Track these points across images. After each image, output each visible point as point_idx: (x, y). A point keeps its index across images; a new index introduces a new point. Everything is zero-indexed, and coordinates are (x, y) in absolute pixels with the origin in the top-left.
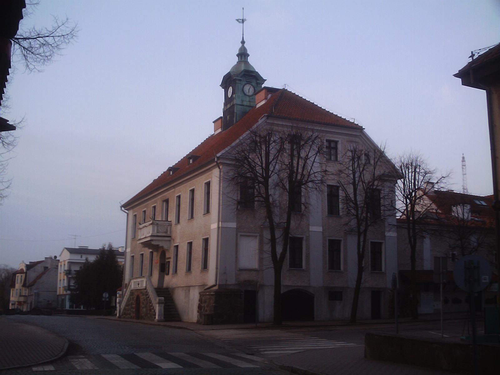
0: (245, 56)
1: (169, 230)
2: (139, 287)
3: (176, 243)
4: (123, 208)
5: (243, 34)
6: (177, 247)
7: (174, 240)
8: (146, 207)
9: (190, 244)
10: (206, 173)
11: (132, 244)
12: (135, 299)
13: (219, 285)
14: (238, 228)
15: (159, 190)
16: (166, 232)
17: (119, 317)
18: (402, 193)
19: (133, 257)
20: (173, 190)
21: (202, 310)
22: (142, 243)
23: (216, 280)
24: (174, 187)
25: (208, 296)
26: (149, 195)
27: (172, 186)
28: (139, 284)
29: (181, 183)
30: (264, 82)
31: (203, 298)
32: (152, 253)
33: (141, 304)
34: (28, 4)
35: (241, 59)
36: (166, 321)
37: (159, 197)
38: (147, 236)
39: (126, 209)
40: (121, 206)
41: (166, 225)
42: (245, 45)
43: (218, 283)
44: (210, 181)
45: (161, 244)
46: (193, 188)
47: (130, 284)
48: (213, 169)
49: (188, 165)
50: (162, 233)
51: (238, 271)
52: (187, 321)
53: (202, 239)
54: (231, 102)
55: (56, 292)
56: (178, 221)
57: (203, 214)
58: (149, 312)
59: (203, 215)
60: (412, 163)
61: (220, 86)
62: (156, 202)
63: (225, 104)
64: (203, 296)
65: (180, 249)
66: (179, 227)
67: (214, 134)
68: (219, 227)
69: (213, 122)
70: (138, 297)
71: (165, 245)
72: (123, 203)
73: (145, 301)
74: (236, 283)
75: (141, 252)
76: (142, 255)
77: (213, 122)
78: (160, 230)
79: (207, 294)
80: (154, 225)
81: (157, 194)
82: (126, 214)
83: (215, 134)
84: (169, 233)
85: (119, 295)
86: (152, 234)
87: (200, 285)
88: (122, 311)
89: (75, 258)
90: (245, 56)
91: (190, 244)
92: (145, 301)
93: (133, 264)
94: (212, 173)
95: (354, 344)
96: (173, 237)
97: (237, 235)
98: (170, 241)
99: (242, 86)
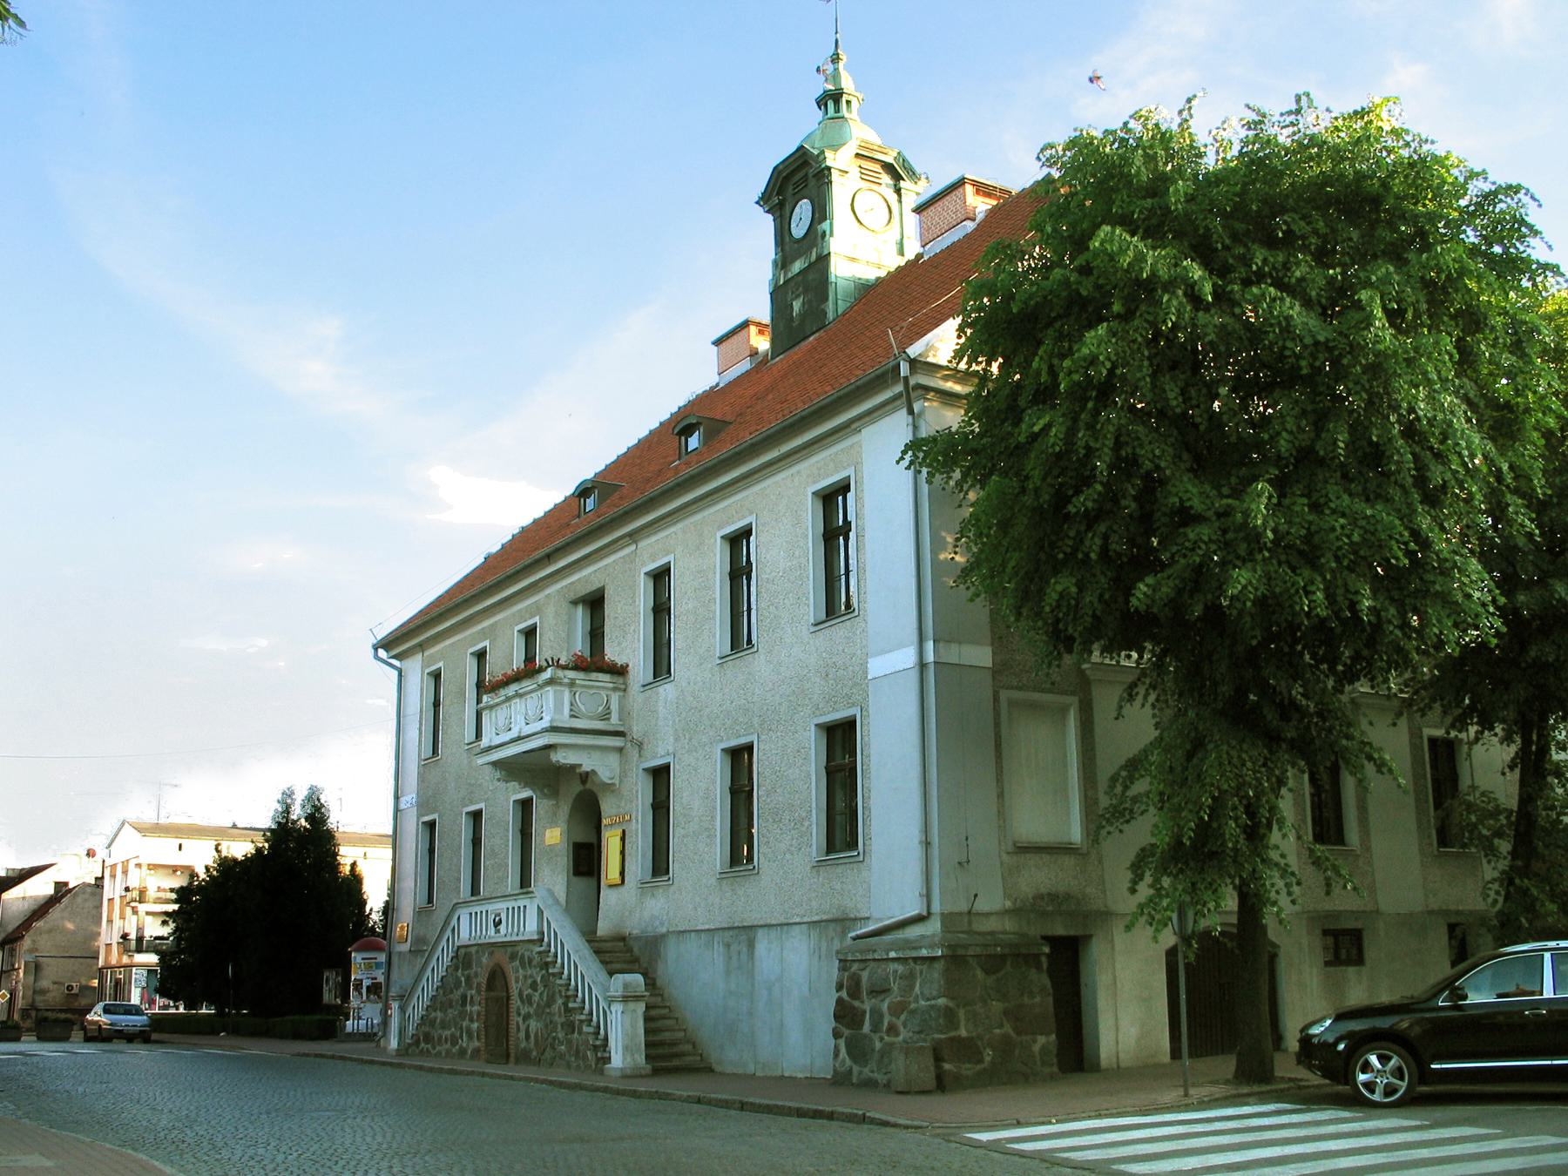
1: (614, 707)
2: (505, 934)
3: (654, 758)
4: (382, 653)
6: (660, 775)
7: (640, 745)
8: (483, 634)
9: (740, 757)
11: (422, 778)
12: (483, 979)
13: (947, 919)
14: (998, 671)
16: (606, 716)
17: (403, 1051)
19: (431, 825)
21: (867, 1028)
22: (495, 764)
23: (928, 896)
24: (633, 536)
25: (900, 968)
28: (497, 924)
31: (865, 975)
32: (525, 806)
33: (515, 1002)
36: (656, 1072)
37: (552, 589)
38: (522, 734)
40: (375, 642)
41: (603, 688)
43: (936, 907)
44: (670, 562)
45: (587, 762)
46: (530, 622)
47: (454, 921)
49: (579, 516)
50: (591, 718)
51: (1008, 853)
52: (779, 1073)
53: (813, 728)
54: (810, 249)
55: (97, 958)
56: (661, 666)
57: (812, 621)
58: (561, 1035)
59: (816, 625)
61: (757, 203)
62: (537, 610)
63: (782, 263)
64: (862, 965)
65: (676, 782)
66: (667, 691)
67: (717, 385)
68: (922, 666)
70: (497, 977)
71: (603, 766)
72: (383, 632)
73: (541, 988)
74: (1008, 904)
75: (472, 803)
76: (476, 816)
78: (582, 707)
79: (893, 954)
80: (561, 684)
81: (541, 579)
82: (396, 673)
83: (721, 385)
84: (614, 719)
85: (1520, 927)
86: (551, 721)
87: (816, 918)
88: (411, 1030)
91: (740, 757)
92: (541, 988)
93: (431, 851)
94: (859, 444)
96: (636, 730)
97: (996, 699)
98: (620, 750)
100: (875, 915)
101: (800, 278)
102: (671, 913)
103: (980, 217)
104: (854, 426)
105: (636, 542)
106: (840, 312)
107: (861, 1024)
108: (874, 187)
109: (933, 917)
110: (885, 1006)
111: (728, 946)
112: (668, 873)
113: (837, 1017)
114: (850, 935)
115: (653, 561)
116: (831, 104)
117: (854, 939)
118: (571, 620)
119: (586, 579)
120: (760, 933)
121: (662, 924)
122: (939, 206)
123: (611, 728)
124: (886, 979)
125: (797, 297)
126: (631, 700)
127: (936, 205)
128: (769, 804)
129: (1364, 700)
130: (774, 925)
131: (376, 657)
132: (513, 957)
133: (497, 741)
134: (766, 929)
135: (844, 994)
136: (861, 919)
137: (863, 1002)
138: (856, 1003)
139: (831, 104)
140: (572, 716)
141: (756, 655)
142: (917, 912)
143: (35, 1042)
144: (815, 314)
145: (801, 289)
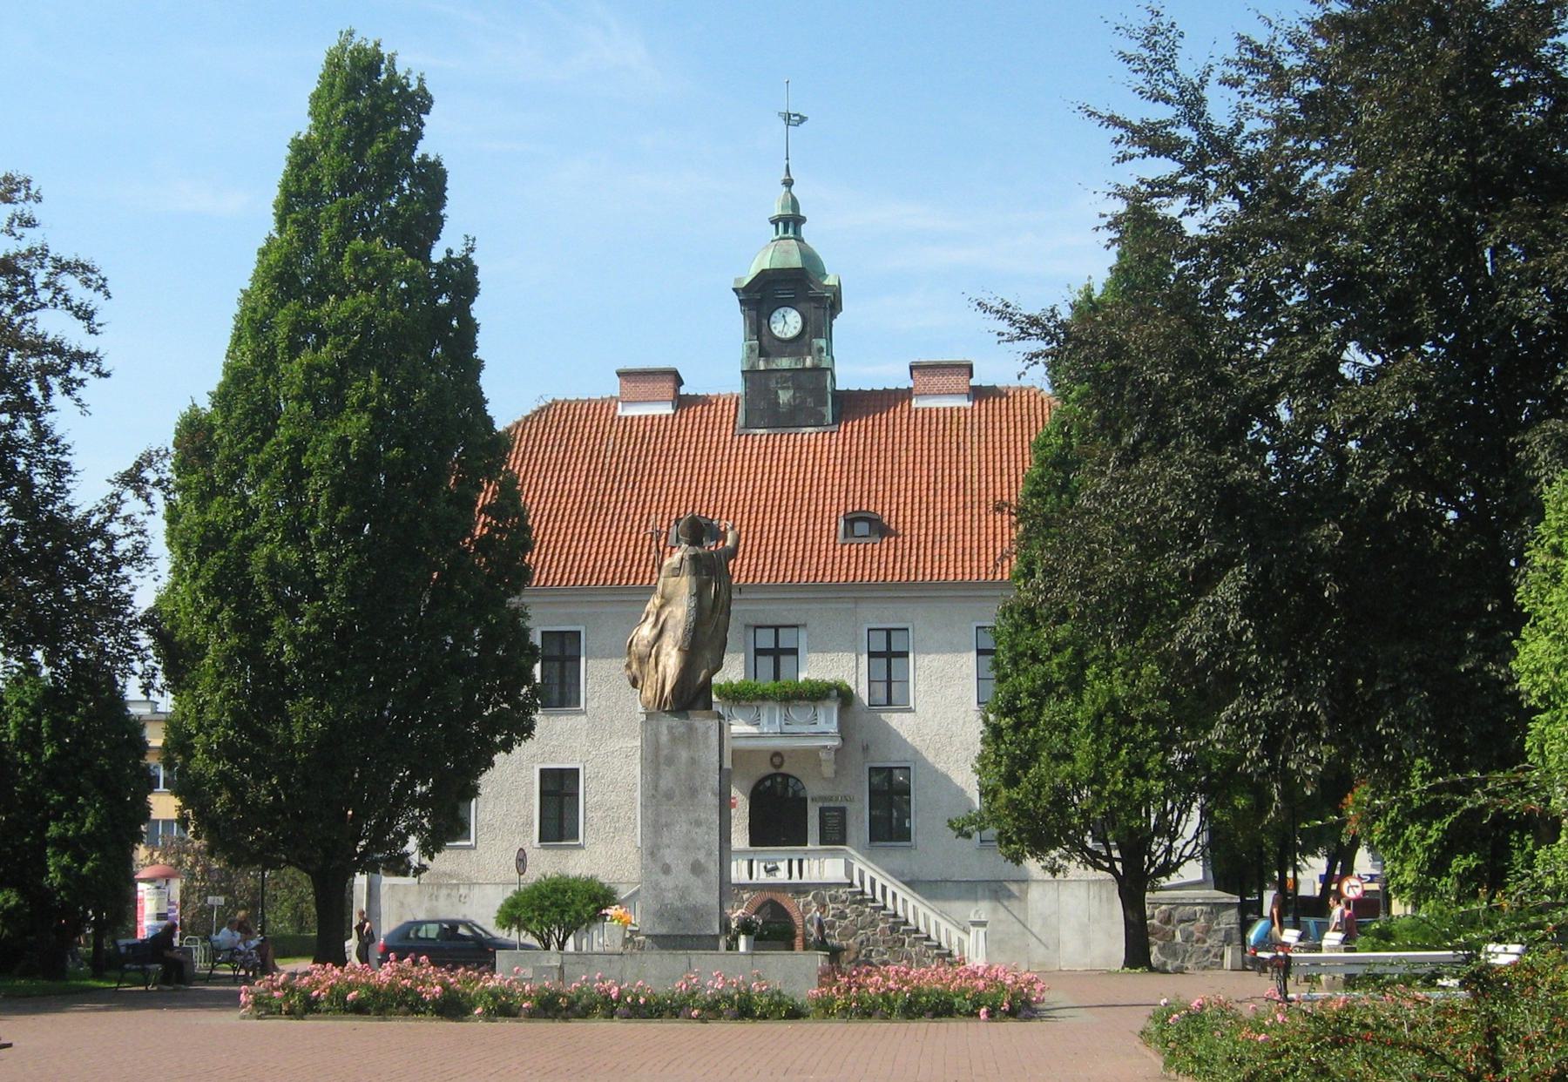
5: (788, 183)
69: (623, 374)
77: (620, 374)
89: (774, 607)
101: (789, 374)
139: (781, 224)
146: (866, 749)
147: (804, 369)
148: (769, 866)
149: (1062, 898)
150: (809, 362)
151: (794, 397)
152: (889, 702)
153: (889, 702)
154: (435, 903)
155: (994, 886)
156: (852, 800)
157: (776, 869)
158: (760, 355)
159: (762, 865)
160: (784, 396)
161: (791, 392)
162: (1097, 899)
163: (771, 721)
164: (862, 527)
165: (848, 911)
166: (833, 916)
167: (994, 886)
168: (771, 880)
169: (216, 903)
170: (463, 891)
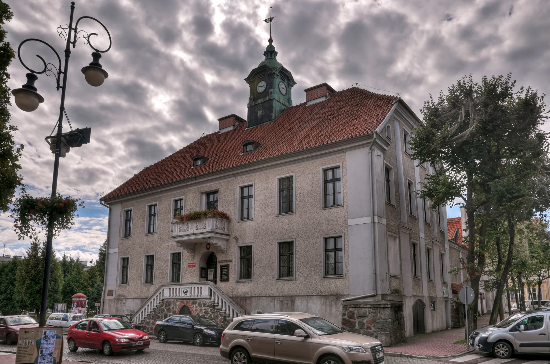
0: (271, 54)
4: (103, 202)
10: (333, 155)
15: (322, 150)
16: (224, 229)
18: (469, 336)
20: (234, 178)
22: (177, 242)
23: (376, 289)
26: (277, 161)
27: (234, 174)
29: (320, 155)
30: (294, 85)
34: (51, 134)
35: (268, 57)
39: (107, 203)
42: (273, 44)
43: (380, 292)
48: (348, 151)
50: (220, 229)
60: (70, 240)
82: (108, 209)
84: (226, 230)
89: (210, 184)
90: (271, 54)
95: (132, 351)
98: (227, 240)
99: (278, 83)
100: (351, 294)
101: (261, 105)
102: (252, 291)
103: (12, 107)
104: (343, 151)
105: (235, 177)
106: (276, 116)
107: (354, 326)
108: (283, 82)
109: (378, 295)
110: (365, 321)
111: (282, 301)
112: (251, 278)
113: (343, 324)
114: (342, 300)
115: (244, 183)
116: (269, 54)
117: (344, 301)
118: (201, 199)
119: (211, 186)
120: (297, 298)
121: (248, 294)
122: (317, 90)
123: (225, 233)
124: (366, 313)
125: (260, 110)
126: (232, 225)
127: (314, 90)
128: (300, 260)
129: (435, 242)
130: (303, 296)
131: (101, 203)
132: (194, 303)
133: (179, 234)
134: (301, 297)
135: (346, 317)
136: (345, 295)
137: (355, 320)
138: (352, 320)
139: (269, 54)
140: (216, 228)
141: (294, 215)
142: (373, 294)
143: (158, 342)
144: (267, 117)
145: (261, 108)
146: (237, 239)
147: (266, 101)
148: (185, 291)
149: (309, 304)
150: (267, 99)
151: (263, 112)
152: (248, 218)
153: (248, 218)
154: (117, 306)
155: (281, 299)
156: (231, 261)
157: (187, 292)
158: (253, 101)
159: (183, 290)
160: (260, 113)
161: (262, 111)
162: (325, 305)
163: (502, 246)
164: (250, 148)
165: (209, 310)
166: (204, 313)
167: (281, 299)
168: (185, 297)
169: (98, 305)
170: (124, 302)
